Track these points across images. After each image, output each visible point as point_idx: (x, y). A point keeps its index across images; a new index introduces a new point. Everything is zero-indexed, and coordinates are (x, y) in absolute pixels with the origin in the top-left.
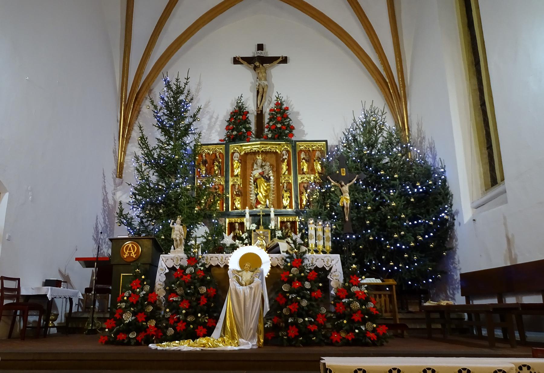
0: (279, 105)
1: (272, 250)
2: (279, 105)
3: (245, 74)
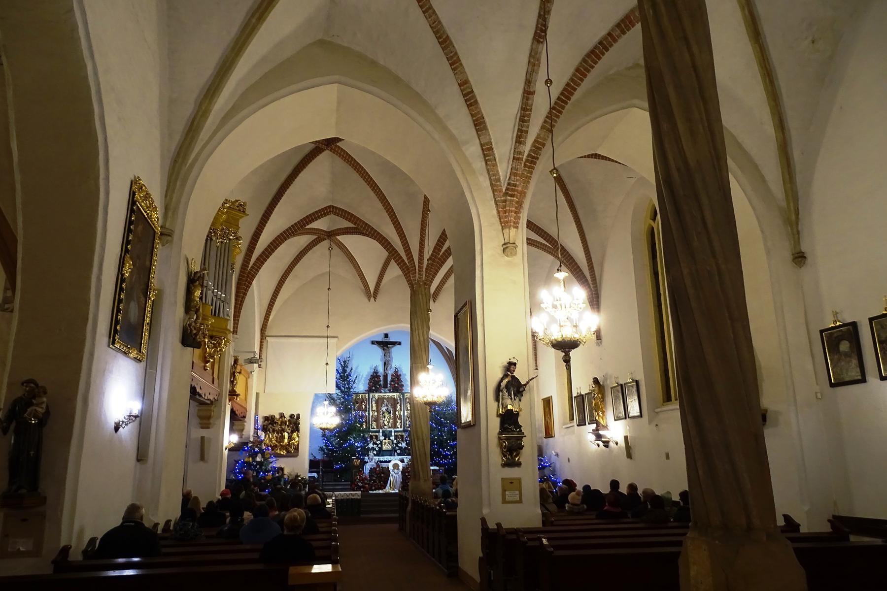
0: (396, 372)
1: (402, 461)
2: (396, 372)
3: (378, 351)
